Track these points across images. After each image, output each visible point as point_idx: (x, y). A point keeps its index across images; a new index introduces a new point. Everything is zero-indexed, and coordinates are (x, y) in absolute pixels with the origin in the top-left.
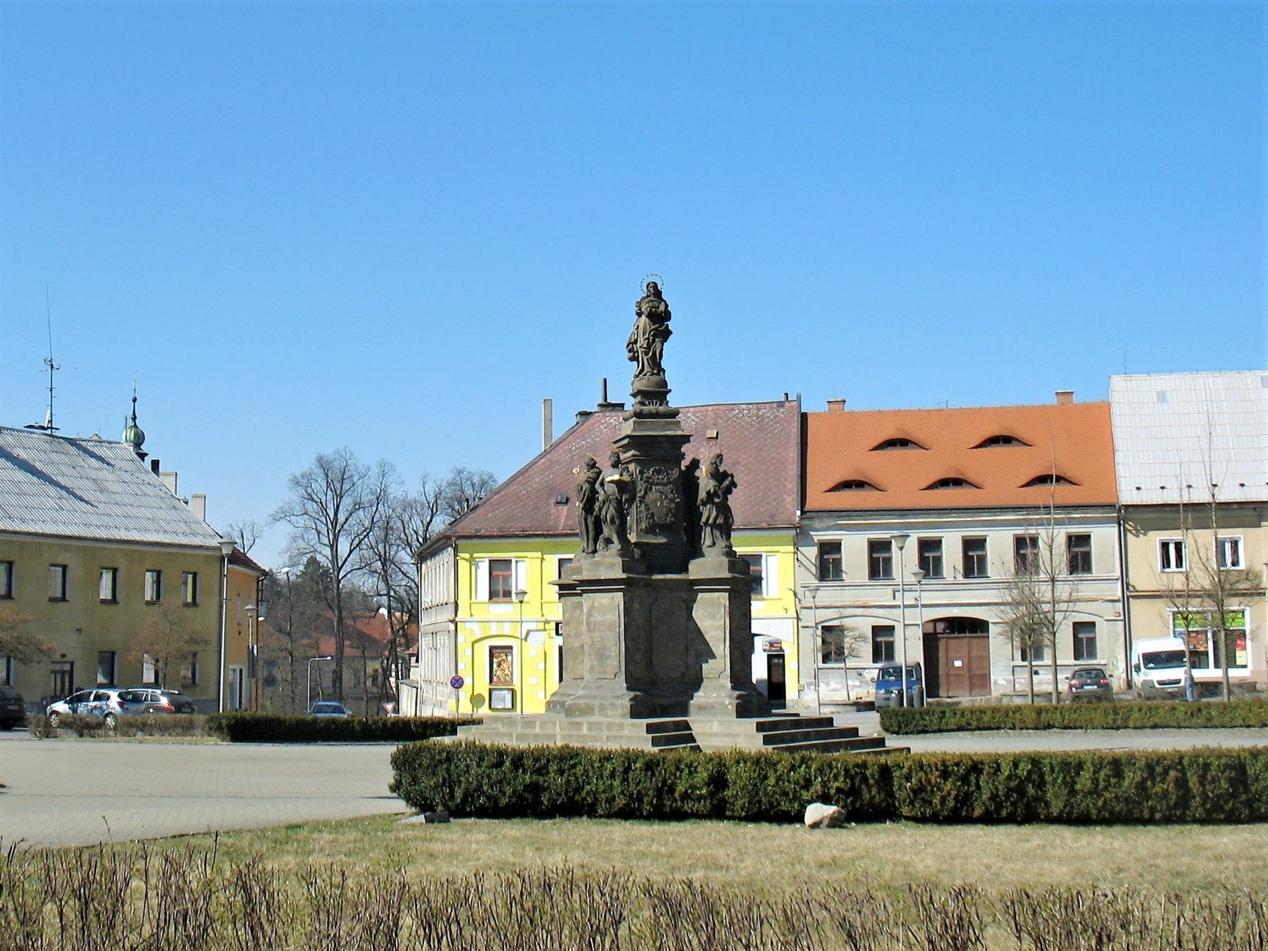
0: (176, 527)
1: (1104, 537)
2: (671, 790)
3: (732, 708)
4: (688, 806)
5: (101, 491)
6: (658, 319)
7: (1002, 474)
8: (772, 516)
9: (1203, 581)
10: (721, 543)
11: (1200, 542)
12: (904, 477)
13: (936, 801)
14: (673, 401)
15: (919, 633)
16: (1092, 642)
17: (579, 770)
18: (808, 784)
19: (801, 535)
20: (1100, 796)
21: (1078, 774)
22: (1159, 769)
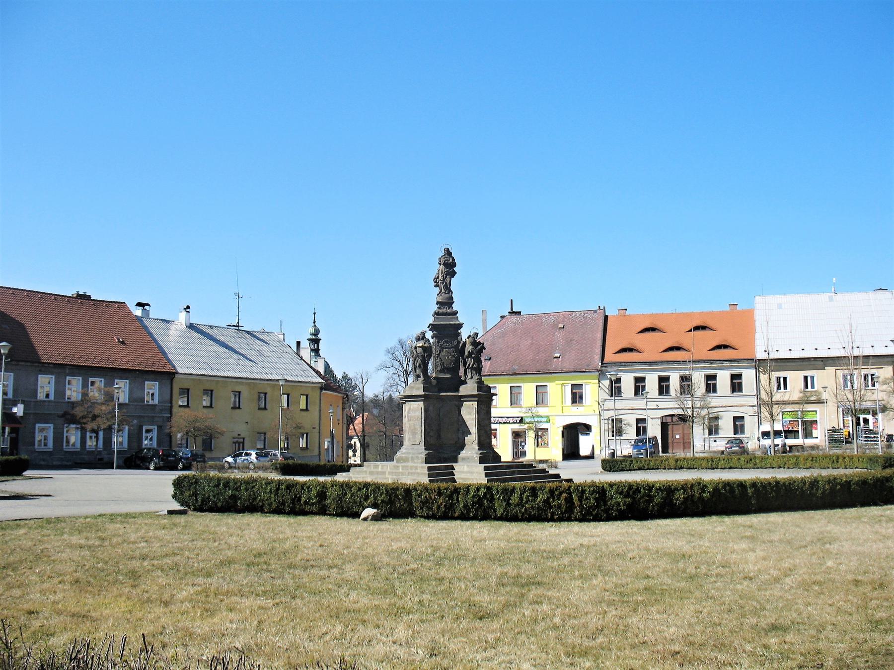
0: (297, 373)
1: (748, 375)
2: (299, 499)
3: (477, 459)
4: (307, 508)
5: (261, 356)
6: (449, 266)
7: (700, 345)
8: (588, 366)
9: (796, 396)
10: (476, 377)
11: (795, 378)
12: (652, 346)
13: (435, 508)
14: (455, 307)
15: (659, 422)
16: (742, 426)
17: (256, 489)
18: (367, 498)
19: (601, 374)
20: (523, 506)
21: (511, 495)
22: (557, 493)
